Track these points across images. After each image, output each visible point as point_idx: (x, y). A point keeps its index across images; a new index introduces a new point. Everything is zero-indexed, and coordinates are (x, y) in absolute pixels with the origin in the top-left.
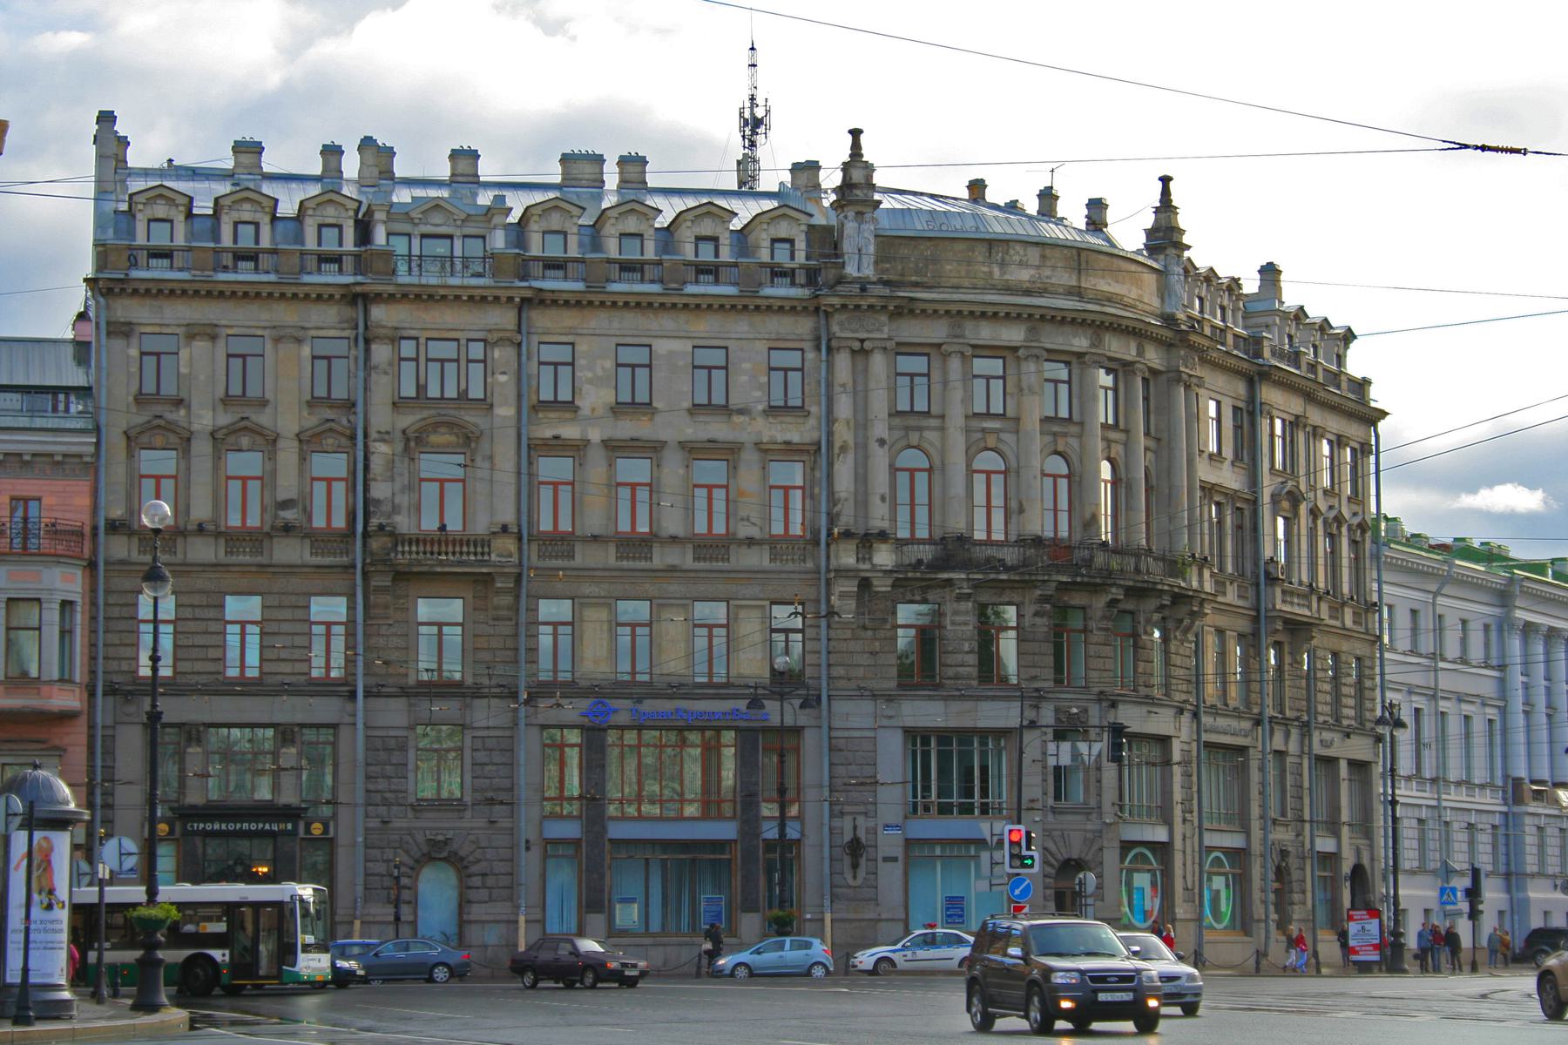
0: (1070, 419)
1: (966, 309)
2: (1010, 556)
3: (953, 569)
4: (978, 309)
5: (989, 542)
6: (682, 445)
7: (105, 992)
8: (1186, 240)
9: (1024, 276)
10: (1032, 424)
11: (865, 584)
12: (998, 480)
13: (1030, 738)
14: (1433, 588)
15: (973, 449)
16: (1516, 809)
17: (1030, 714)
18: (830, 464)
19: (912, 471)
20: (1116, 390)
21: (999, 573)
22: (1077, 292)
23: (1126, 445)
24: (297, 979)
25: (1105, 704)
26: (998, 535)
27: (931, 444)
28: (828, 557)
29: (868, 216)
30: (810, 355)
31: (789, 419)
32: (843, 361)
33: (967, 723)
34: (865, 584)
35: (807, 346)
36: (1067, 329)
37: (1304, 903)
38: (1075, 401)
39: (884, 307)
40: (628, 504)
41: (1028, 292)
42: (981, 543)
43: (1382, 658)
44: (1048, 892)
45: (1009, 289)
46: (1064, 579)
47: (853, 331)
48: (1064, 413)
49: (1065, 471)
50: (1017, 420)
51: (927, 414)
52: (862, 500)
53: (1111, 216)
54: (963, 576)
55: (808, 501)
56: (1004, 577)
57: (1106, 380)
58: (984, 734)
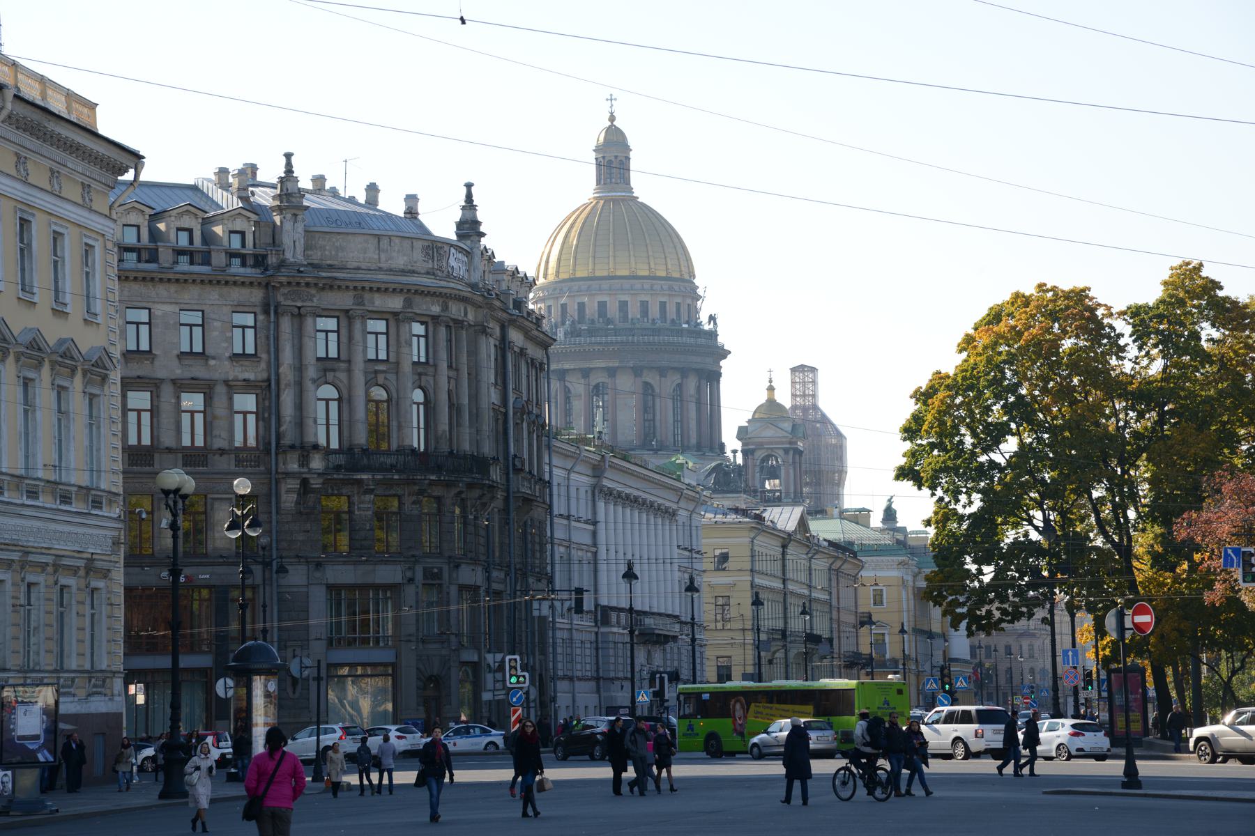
0: (427, 363)
1: (367, 285)
3: (363, 470)
4: (375, 286)
6: (174, 381)
8: (482, 229)
10: (407, 368)
11: (305, 483)
13: (410, 591)
16: (603, 630)
17: (409, 574)
18: (278, 396)
20: (426, 336)
24: (416, 762)
28: (277, 464)
29: (300, 218)
30: (261, 317)
31: (246, 363)
32: (286, 324)
33: (369, 580)
34: (305, 483)
35: (258, 310)
39: (316, 285)
40: (196, 431)
46: (433, 477)
48: (382, 356)
50: (398, 363)
51: (338, 359)
52: (300, 423)
53: (421, 208)
55: (261, 423)
57: (418, 329)
58: (377, 587)
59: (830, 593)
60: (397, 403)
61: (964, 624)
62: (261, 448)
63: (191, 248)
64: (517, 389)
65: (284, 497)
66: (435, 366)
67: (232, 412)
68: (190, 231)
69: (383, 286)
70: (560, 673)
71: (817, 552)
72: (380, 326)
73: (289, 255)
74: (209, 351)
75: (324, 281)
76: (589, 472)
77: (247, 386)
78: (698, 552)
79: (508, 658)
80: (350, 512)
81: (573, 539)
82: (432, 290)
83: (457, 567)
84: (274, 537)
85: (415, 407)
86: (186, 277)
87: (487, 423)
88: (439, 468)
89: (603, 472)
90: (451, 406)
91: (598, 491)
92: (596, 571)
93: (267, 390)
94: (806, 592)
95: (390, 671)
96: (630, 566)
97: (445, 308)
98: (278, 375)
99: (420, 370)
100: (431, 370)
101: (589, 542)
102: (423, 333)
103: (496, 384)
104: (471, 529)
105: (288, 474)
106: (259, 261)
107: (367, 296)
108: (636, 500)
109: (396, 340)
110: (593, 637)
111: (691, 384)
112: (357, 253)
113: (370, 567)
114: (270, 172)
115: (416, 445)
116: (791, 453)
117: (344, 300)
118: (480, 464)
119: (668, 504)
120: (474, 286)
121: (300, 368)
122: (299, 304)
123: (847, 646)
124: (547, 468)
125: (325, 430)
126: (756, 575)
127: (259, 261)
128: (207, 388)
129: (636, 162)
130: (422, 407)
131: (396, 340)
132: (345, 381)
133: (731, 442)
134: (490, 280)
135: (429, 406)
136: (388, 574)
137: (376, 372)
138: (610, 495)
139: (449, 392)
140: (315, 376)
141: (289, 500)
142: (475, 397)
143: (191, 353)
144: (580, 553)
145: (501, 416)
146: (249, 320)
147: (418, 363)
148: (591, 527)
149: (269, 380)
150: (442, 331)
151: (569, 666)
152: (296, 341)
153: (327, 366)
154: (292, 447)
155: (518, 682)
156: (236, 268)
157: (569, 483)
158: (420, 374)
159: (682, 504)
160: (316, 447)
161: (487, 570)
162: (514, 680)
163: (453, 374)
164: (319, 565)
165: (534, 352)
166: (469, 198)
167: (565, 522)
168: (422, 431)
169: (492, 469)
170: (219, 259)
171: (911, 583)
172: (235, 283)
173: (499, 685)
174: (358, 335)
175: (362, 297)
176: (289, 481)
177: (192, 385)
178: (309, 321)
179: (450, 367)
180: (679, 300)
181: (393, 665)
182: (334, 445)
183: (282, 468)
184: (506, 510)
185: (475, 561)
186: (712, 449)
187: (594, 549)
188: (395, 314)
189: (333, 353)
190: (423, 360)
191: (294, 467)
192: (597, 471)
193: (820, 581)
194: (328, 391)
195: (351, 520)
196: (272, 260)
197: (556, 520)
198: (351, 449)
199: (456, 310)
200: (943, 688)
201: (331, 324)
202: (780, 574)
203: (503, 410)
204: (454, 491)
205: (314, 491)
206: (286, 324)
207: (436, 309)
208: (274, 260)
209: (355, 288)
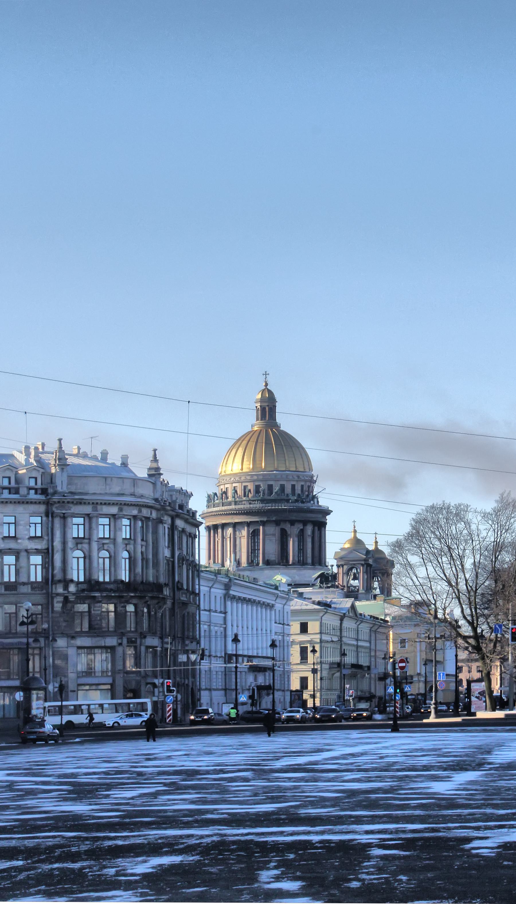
0: (130, 538)
1: (99, 502)
2: (112, 586)
4: (103, 502)
5: (104, 583)
10: (119, 540)
11: (66, 599)
17: (120, 641)
22: (133, 495)
26: (107, 579)
29: (65, 470)
30: (44, 519)
32: (57, 522)
34: (66, 599)
35: (43, 515)
36: (131, 507)
46: (132, 595)
47: (61, 510)
48: (107, 536)
50: (115, 539)
51: (84, 538)
53: (129, 461)
54: (99, 595)
55: (44, 570)
62: (44, 581)
63: (10, 486)
64: (180, 549)
65: (56, 605)
66: (135, 540)
67: (29, 565)
68: (9, 478)
70: (203, 687)
71: (362, 622)
72: (106, 521)
73: (59, 489)
74: (17, 536)
76: (223, 587)
77: (38, 552)
78: (288, 625)
79: (166, 681)
82: (133, 503)
84: (51, 625)
85: (123, 560)
86: (7, 500)
87: (163, 567)
88: (135, 590)
89: (230, 587)
90: (143, 559)
91: (227, 597)
92: (210, 641)
93: (47, 554)
94: (355, 643)
96: (236, 636)
97: (140, 511)
98: (53, 546)
99: (126, 542)
101: (222, 622)
102: (128, 524)
103: (168, 547)
104: (153, 619)
105: (58, 594)
106: (44, 491)
107: (99, 507)
108: (249, 600)
109: (115, 528)
110: (223, 670)
112: (94, 487)
114: (52, 446)
115: (124, 579)
116: (365, 566)
117: (88, 509)
118: (158, 587)
119: (269, 601)
120: (156, 500)
121: (64, 543)
122: (64, 512)
124: (197, 587)
125: (77, 572)
126: (323, 635)
127: (44, 491)
128: (17, 553)
129: (279, 408)
130: (127, 561)
131: (115, 528)
133: (331, 560)
134: (166, 496)
135: (132, 560)
137: (103, 544)
138: (233, 598)
139: (142, 553)
140: (72, 547)
141: (58, 606)
142: (156, 554)
143: (9, 537)
144: (216, 628)
145: (171, 563)
146: (38, 520)
147: (126, 539)
148: (223, 615)
149: (48, 549)
150: (140, 524)
152: (62, 529)
153: (78, 541)
154: (59, 581)
156: (32, 495)
157: (210, 594)
158: (126, 544)
159: (278, 601)
160: (72, 581)
161: (161, 638)
163: (144, 543)
165: (189, 529)
166: (155, 455)
167: (207, 613)
168: (127, 572)
169: (164, 589)
170: (23, 491)
172: (31, 503)
173: (161, 694)
174: (94, 525)
175: (96, 507)
176: (58, 597)
177: (10, 552)
178: (69, 520)
179: (142, 540)
180: (303, 483)
182: (82, 579)
183: (54, 591)
184: (172, 610)
185: (154, 634)
187: (224, 626)
189: (81, 535)
191: (60, 590)
192: (227, 587)
194: (79, 553)
196: (50, 491)
197: (202, 612)
199: (145, 512)
201: (81, 520)
203: (172, 560)
205: (71, 602)
206: (57, 522)
207: (135, 512)
208: (52, 491)
209: (93, 503)
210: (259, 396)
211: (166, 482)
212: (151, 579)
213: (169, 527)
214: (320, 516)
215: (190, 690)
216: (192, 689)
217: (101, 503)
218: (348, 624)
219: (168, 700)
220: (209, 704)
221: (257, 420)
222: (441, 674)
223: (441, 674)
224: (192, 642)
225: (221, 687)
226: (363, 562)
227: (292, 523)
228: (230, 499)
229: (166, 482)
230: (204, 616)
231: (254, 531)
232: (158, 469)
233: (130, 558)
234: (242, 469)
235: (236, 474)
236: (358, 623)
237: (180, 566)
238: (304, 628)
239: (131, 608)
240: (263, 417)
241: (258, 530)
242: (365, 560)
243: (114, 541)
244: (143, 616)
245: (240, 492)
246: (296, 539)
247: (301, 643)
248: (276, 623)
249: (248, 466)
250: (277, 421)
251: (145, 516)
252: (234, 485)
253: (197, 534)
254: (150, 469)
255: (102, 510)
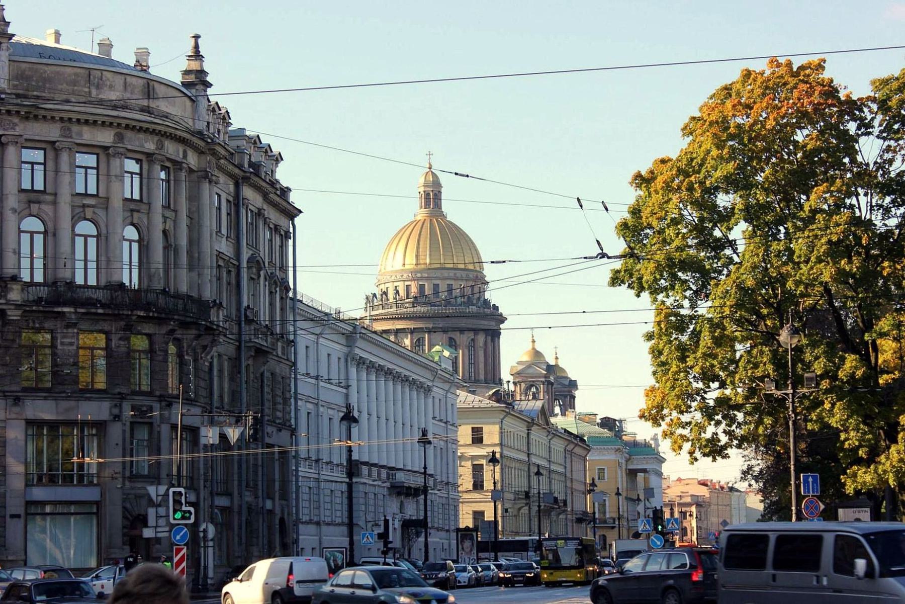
0: (141, 201)
1: (75, 116)
2: (99, 295)
3: (65, 304)
4: (83, 117)
5: (86, 286)
7: (125, 530)
8: (208, 79)
9: (113, 96)
10: (117, 203)
12: (92, 242)
13: (116, 432)
14: (318, 330)
15: (76, 218)
17: (116, 411)
19: (32, 233)
20: (141, 174)
21: (97, 308)
23: (175, 221)
25: (164, 404)
26: (92, 281)
27: (47, 214)
36: (142, 136)
37: (257, 545)
38: (144, 188)
39: (18, 112)
41: (115, 107)
42: (80, 286)
43: (296, 379)
44: (125, 539)
45: (101, 103)
46: (142, 314)
48: (92, 190)
49: (136, 237)
51: (44, 192)
56: (100, 311)
57: (131, 165)
59: (565, 467)
60: (107, 237)
61: (687, 446)
69: (91, 118)
70: (305, 518)
72: (90, 160)
75: (26, 109)
78: (453, 425)
79: (172, 490)
80: (53, 346)
81: (321, 398)
83: (170, 405)
85: (126, 245)
89: (355, 341)
90: (166, 248)
91: (350, 359)
95: (95, 511)
97: (160, 146)
100: (144, 208)
102: (138, 171)
107: (75, 128)
111: (481, 338)
113: (72, 403)
117: (52, 132)
123: (578, 507)
130: (135, 246)
132: (51, 214)
133: (506, 375)
135: (144, 245)
136: (90, 411)
137: (84, 206)
142: (194, 242)
148: (344, 391)
151: (316, 512)
153: (32, 199)
155: (183, 518)
162: (178, 515)
163: (169, 214)
164: (17, 400)
166: (196, 47)
171: (624, 467)
173: (162, 522)
174: (64, 166)
175: (69, 129)
181: (97, 503)
182: (39, 278)
184: (236, 362)
186: (494, 382)
188: (106, 148)
189: (39, 186)
190: (136, 196)
193: (558, 457)
194: (32, 224)
195: (54, 354)
198: (55, 283)
200: (656, 529)
202: (525, 449)
204: (164, 330)
207: (150, 146)
209: (62, 119)
210: (422, 180)
211: (223, 111)
212: (184, 288)
213: (231, 199)
214: (493, 323)
215: (277, 522)
216: (282, 520)
217: (78, 121)
218: (538, 435)
219: (178, 537)
220: (317, 551)
221: (421, 207)
222: (810, 480)
223: (810, 480)
224: (280, 430)
225: (339, 520)
226: (543, 379)
227: (462, 331)
228: (391, 300)
229: (223, 111)
230: (305, 387)
231: (419, 340)
232: (201, 73)
233: (140, 241)
234: (404, 265)
235: (397, 271)
236: (550, 437)
237: (253, 279)
238: (477, 438)
239: (140, 343)
240: (427, 205)
241: (423, 338)
242: (546, 376)
243: (105, 203)
244: (166, 361)
245: (402, 293)
246: (466, 351)
247: (473, 458)
248: (434, 418)
249: (411, 260)
250: (443, 209)
251: (173, 157)
252: (396, 284)
253: (291, 230)
254: (186, 73)
255: (80, 134)
